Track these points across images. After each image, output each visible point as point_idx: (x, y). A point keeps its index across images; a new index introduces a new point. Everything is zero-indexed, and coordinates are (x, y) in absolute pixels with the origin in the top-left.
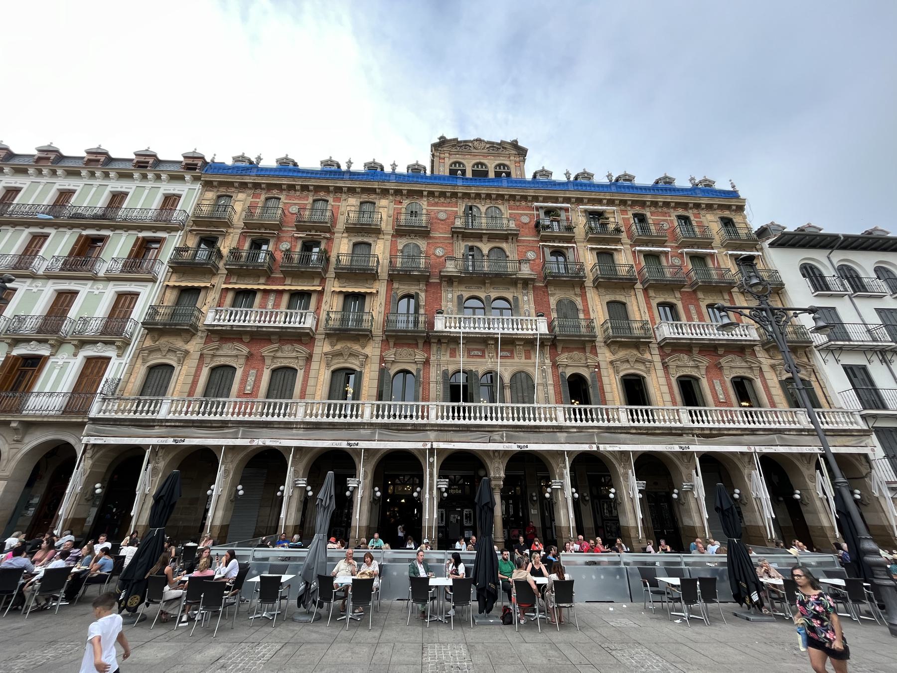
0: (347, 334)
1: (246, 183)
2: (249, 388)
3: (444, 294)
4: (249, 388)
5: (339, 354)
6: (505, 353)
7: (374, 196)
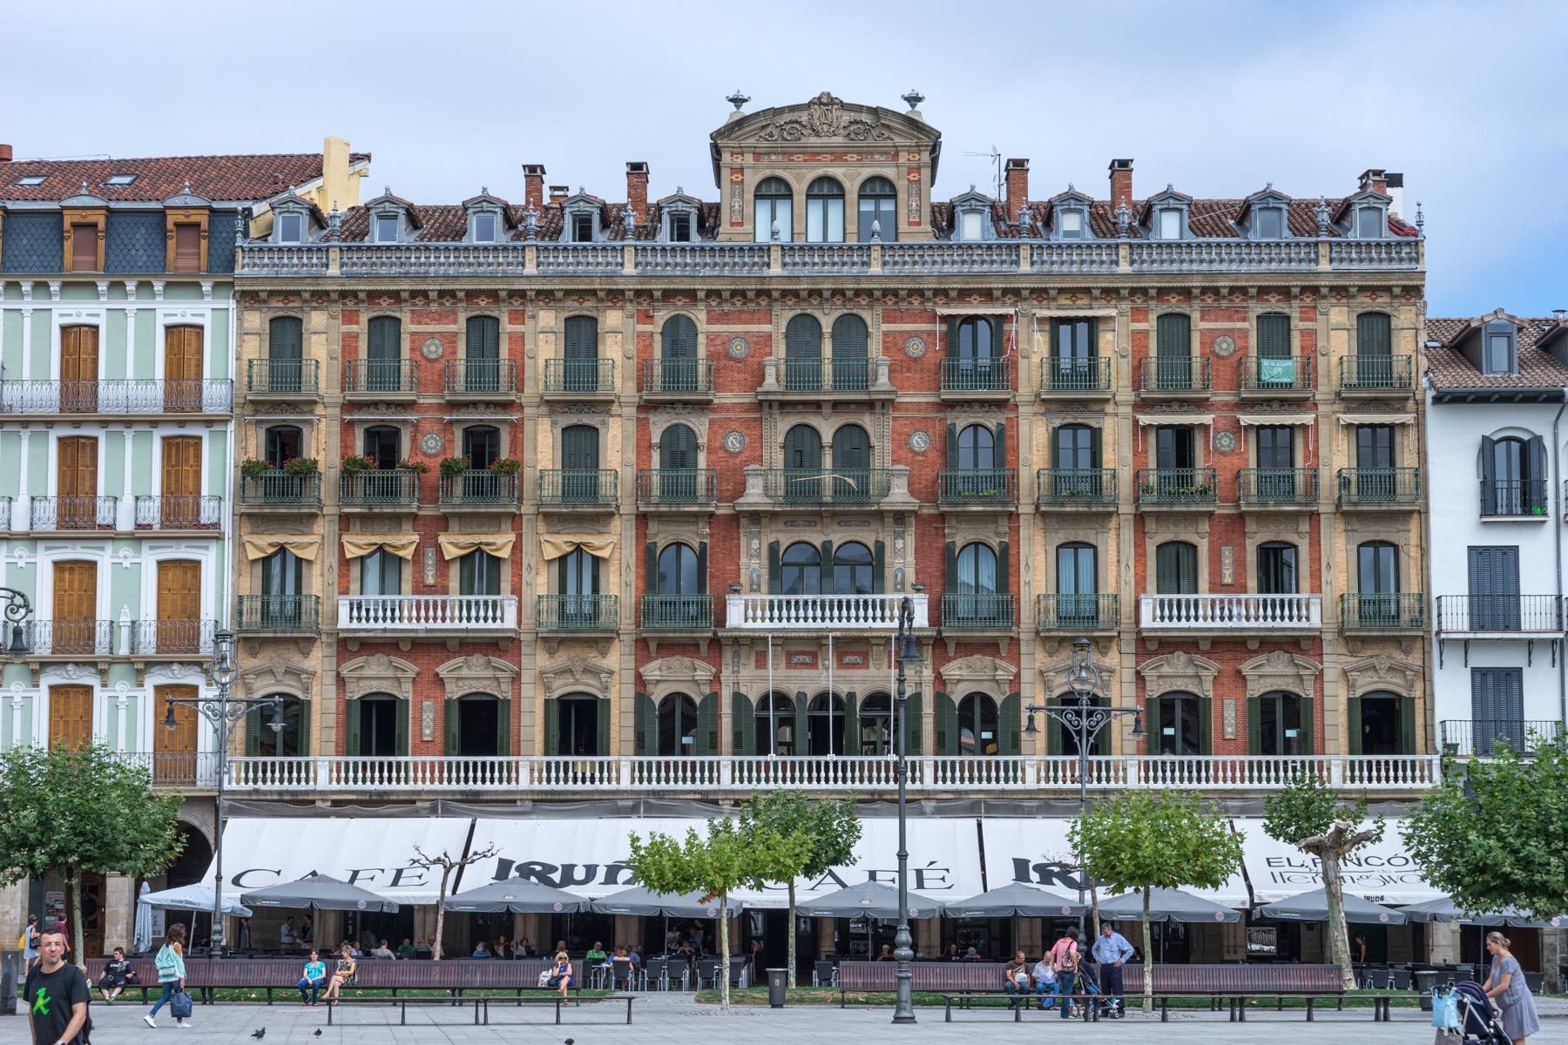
1: (327, 293)
2: (1229, 730)
3: (743, 541)
4: (427, 731)
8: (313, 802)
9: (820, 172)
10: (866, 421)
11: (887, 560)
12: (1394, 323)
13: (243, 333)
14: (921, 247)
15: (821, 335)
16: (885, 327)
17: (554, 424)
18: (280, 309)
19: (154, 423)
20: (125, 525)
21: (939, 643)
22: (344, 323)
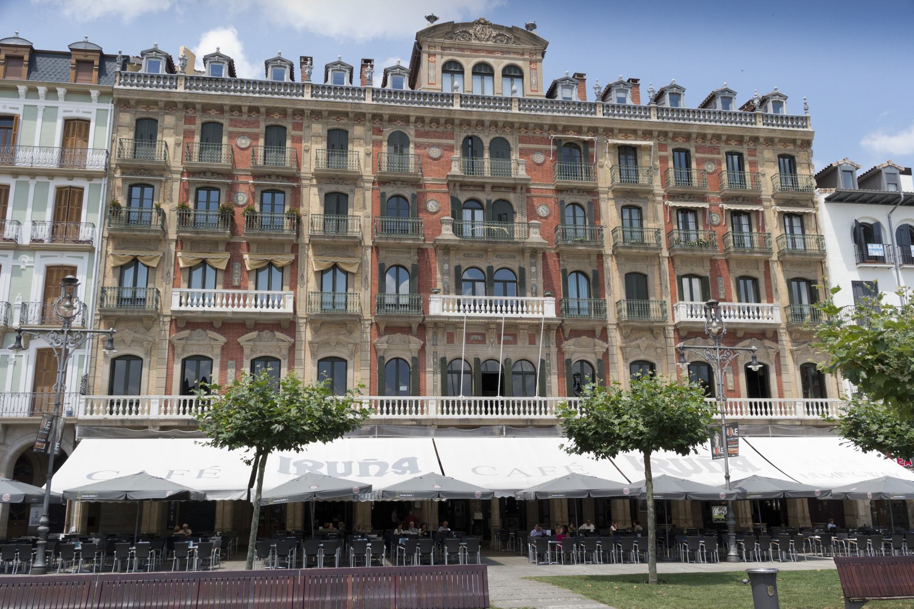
0: (334, 321)
2: (730, 384)
5: (327, 343)
6: (508, 338)
7: (344, 121)
8: (147, 427)
9: (481, 60)
10: (511, 197)
11: (527, 280)
12: (797, 159)
13: (116, 127)
14: (535, 101)
15: (490, 149)
16: (520, 145)
17: (320, 190)
18: (144, 113)
19: (51, 174)
20: (25, 241)
21: (560, 328)
22: (185, 123)
